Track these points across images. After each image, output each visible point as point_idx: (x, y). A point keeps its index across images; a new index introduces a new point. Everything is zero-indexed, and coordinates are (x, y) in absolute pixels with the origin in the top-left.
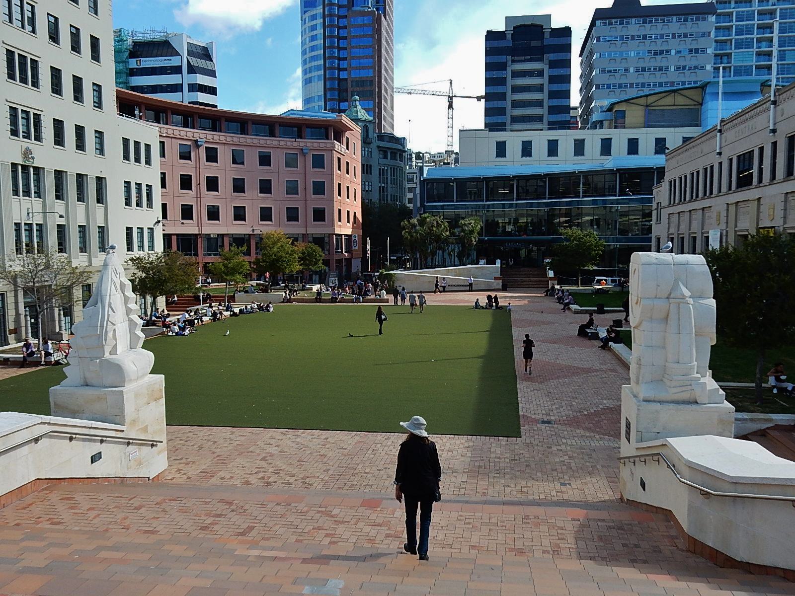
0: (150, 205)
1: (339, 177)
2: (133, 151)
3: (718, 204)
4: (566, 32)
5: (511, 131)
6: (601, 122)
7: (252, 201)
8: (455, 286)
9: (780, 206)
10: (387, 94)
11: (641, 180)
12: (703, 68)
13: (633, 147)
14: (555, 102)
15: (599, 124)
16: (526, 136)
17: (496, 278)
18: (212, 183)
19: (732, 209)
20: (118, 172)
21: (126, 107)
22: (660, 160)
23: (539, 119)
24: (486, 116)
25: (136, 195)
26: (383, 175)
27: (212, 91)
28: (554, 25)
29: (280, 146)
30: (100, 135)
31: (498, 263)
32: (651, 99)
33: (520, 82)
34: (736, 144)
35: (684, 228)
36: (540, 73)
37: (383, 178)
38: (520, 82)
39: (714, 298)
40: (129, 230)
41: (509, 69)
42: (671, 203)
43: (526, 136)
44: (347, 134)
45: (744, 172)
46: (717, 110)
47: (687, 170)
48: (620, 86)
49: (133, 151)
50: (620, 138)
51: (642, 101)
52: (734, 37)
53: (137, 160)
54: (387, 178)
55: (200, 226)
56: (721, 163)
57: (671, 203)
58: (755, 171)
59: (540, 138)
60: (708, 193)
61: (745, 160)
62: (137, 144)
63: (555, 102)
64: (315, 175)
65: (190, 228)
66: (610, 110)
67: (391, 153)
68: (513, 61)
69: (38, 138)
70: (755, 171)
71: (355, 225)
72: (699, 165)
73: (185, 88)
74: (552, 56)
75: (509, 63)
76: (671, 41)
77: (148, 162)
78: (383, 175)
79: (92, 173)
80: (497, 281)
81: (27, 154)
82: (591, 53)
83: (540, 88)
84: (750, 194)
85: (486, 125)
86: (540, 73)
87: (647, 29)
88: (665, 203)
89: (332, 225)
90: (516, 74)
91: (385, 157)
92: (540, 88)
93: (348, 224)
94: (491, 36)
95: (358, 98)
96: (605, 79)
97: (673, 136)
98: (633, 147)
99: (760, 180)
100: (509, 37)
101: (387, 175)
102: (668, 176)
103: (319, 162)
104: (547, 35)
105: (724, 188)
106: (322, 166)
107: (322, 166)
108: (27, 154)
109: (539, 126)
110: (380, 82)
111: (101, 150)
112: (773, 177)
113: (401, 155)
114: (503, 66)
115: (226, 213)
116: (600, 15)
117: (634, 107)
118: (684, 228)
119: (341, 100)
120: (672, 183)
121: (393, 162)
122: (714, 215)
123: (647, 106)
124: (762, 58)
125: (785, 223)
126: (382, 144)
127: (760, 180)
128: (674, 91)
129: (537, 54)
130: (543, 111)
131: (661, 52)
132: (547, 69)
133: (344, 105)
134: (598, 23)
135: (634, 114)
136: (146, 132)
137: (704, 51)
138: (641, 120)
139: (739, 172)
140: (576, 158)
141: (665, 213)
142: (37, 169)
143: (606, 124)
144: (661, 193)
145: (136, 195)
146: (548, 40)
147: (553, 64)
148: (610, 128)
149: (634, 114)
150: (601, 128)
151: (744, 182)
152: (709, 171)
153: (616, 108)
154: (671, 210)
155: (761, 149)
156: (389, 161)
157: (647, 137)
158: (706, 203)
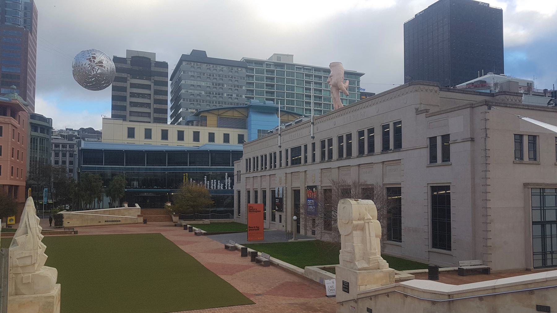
3: (280, 173)
4: (165, 65)
5: (130, 121)
8: (110, 221)
10: (31, 86)
11: (227, 158)
12: (241, 96)
13: (212, 137)
16: (148, 126)
17: (139, 216)
22: (240, 147)
24: (112, 110)
26: (34, 143)
28: (157, 59)
32: (221, 112)
33: (135, 90)
36: (148, 87)
37: (34, 145)
38: (135, 90)
39: (48, 263)
40: (534, 158)
41: (128, 82)
43: (148, 126)
44: (20, 113)
45: (296, 156)
46: (258, 121)
50: (204, 132)
51: (216, 112)
52: (255, 81)
54: (37, 146)
56: (281, 152)
58: (302, 156)
59: (157, 129)
60: (273, 166)
61: (296, 151)
67: (41, 128)
70: (302, 156)
71: (12, 177)
74: (156, 78)
75: (129, 78)
78: (34, 143)
80: (139, 218)
82: (180, 80)
84: (300, 169)
85: (113, 116)
88: (243, 171)
90: (133, 86)
91: (36, 131)
93: (239, 189)
95: (15, 87)
97: (234, 133)
98: (212, 137)
99: (306, 161)
100: (129, 62)
101: (37, 143)
102: (245, 157)
104: (153, 65)
105: (284, 164)
112: (314, 160)
113: (48, 131)
114: (125, 80)
116: (184, 59)
120: (248, 161)
121: (42, 135)
123: (219, 115)
124: (269, 95)
125: (321, 184)
126: (34, 121)
127: (306, 161)
128: (233, 108)
129: (148, 75)
132: (152, 85)
134: (184, 63)
135: (212, 119)
137: (241, 87)
138: (215, 123)
139: (292, 157)
140: (179, 142)
141: (243, 178)
143: (195, 122)
144: (239, 166)
146: (153, 69)
147: (157, 83)
148: (197, 125)
150: (192, 125)
151: (296, 162)
152: (273, 156)
154: (248, 175)
155: (306, 146)
156: (38, 134)
157: (219, 133)
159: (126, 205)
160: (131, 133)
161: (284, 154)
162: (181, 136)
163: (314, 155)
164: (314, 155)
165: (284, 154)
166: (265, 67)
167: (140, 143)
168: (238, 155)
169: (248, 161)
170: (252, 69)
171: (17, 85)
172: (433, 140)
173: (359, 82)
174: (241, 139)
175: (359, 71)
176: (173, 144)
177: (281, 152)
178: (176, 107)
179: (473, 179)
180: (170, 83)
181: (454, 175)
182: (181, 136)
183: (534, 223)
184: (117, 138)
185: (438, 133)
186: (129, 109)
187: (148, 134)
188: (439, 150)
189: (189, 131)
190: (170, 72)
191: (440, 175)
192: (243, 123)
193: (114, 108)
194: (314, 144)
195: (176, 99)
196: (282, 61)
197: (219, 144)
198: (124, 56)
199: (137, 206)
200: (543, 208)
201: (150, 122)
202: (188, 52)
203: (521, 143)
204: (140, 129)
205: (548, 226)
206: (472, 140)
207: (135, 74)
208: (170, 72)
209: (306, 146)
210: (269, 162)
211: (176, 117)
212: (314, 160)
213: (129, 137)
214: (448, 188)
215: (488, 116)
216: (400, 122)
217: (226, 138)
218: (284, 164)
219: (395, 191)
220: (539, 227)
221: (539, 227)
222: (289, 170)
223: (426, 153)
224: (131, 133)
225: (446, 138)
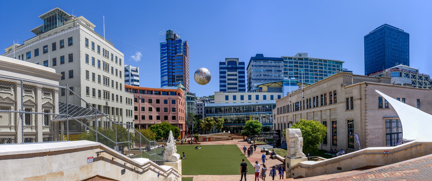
0: (132, 116)
1: (180, 106)
2: (128, 101)
4: (243, 63)
6: (256, 90)
7: (154, 114)
9: (306, 116)
13: (265, 98)
14: (241, 84)
15: (255, 91)
18: (143, 109)
19: (294, 116)
20: (124, 106)
21: (127, 89)
22: (274, 102)
23: (236, 88)
25: (129, 113)
27: (138, 81)
29: (154, 97)
30: (121, 97)
31: (229, 132)
32: (269, 84)
33: (230, 77)
34: (294, 100)
35: (282, 121)
36: (236, 75)
42: (278, 114)
47: (282, 105)
48: (259, 79)
49: (128, 101)
50: (261, 95)
51: (267, 85)
53: (129, 103)
55: (140, 121)
57: (278, 114)
59: (238, 95)
62: (129, 99)
63: (241, 84)
64: (172, 106)
65: (143, 122)
66: (258, 87)
68: (228, 71)
69: (109, 99)
72: (285, 104)
73: (130, 81)
74: (239, 70)
76: (273, 68)
77: (131, 104)
79: (115, 106)
81: (107, 103)
83: (236, 80)
84: (299, 112)
85: (221, 90)
86: (236, 75)
87: (266, 64)
88: (276, 114)
89: (178, 121)
90: (229, 75)
92: (236, 80)
94: (221, 63)
96: (254, 77)
97: (276, 95)
98: (265, 98)
99: (301, 109)
100: (226, 64)
102: (278, 106)
103: (174, 102)
104: (238, 64)
105: (292, 111)
106: (175, 103)
107: (175, 103)
108: (107, 103)
109: (235, 90)
110: (185, 76)
111: (121, 101)
115: (147, 118)
116: (253, 59)
117: (264, 86)
118: (282, 121)
119: (173, 82)
120: (278, 109)
122: (290, 118)
129: (235, 69)
130: (237, 86)
131: (270, 70)
133: (174, 83)
134: (252, 61)
136: (131, 96)
142: (108, 107)
144: (275, 111)
145: (129, 113)
146: (238, 66)
147: (240, 73)
149: (265, 88)
151: (297, 109)
152: (288, 106)
153: (260, 86)
154: (278, 116)
155: (301, 102)
157: (268, 95)
158: (287, 114)
159: (224, 132)
160: (227, 98)
161: (292, 105)
162: (250, 97)
163: (304, 106)
164: (304, 106)
165: (292, 105)
166: (293, 60)
167: (231, 103)
168: (274, 106)
169: (278, 109)
170: (287, 62)
171: (182, 80)
172: (347, 99)
173: (342, 66)
174: (279, 97)
175: (342, 61)
176: (246, 102)
177: (304, 101)
178: (250, 83)
179: (361, 116)
180: (246, 71)
181: (355, 114)
182: (250, 97)
183: (387, 134)
184: (220, 101)
185: (349, 96)
186: (228, 86)
187: (235, 98)
188: (350, 104)
189: (253, 95)
190: (246, 67)
191: (350, 115)
192: (280, 90)
193: (221, 86)
194: (304, 101)
195: (250, 79)
196: (302, 57)
197: (269, 101)
198: (224, 61)
199: (229, 132)
200: (391, 128)
201: (237, 92)
202: (254, 55)
203: (325, 103)
204: (231, 95)
205: (393, 135)
206: (361, 99)
207: (229, 69)
208: (246, 67)
209: (301, 102)
210: (285, 110)
211: (250, 88)
212: (304, 109)
213: (241, 99)
214: (353, 121)
215: (367, 89)
216: (336, 91)
217: (272, 98)
218: (292, 111)
219: (334, 122)
220: (389, 135)
221: (389, 135)
222: (294, 113)
223: (344, 105)
224: (227, 98)
225: (352, 98)
